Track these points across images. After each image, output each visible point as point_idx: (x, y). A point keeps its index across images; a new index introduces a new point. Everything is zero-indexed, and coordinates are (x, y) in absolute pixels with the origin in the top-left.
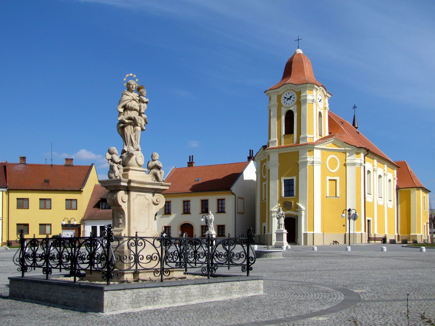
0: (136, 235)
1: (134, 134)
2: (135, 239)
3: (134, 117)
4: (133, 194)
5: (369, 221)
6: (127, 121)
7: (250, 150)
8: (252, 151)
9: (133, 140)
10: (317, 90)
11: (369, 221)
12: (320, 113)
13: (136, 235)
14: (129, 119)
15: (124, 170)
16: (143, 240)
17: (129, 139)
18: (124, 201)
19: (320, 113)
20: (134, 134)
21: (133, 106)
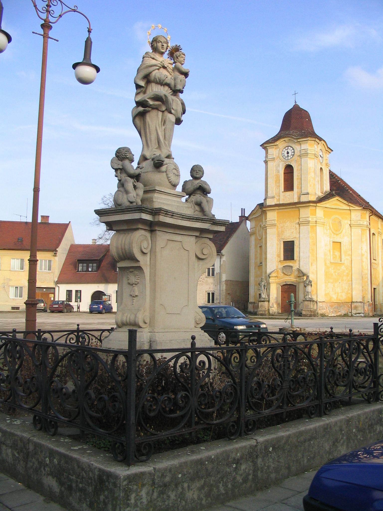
0: (193, 344)
1: (164, 127)
2: (189, 354)
3: (165, 95)
4: (162, 237)
5: (374, 289)
6: (151, 102)
7: (242, 209)
8: (244, 209)
9: (162, 138)
10: (319, 144)
11: (374, 289)
12: (321, 169)
13: (193, 344)
14: (157, 98)
15: (145, 192)
16: (207, 355)
17: (154, 136)
18: (145, 251)
19: (321, 169)
20: (164, 127)
21: (163, 78)
